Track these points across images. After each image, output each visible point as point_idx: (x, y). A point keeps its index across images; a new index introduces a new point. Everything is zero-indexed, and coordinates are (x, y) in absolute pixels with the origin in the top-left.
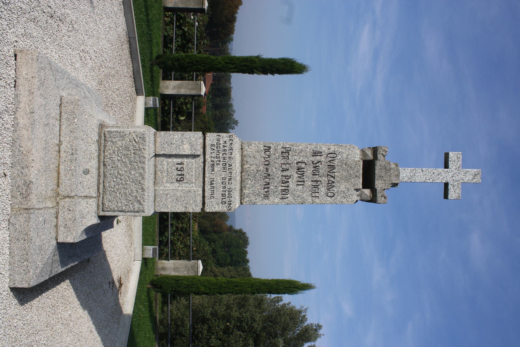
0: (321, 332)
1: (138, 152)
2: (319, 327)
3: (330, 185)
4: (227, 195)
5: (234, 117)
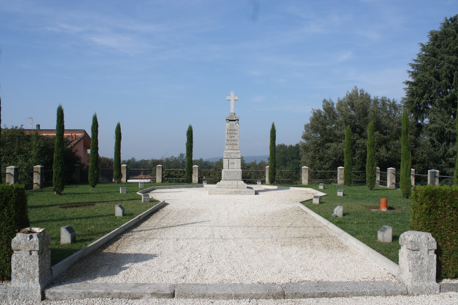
0: (328, 100)
1: (228, 172)
2: (325, 101)
3: (235, 130)
4: (237, 153)
5: (177, 157)
